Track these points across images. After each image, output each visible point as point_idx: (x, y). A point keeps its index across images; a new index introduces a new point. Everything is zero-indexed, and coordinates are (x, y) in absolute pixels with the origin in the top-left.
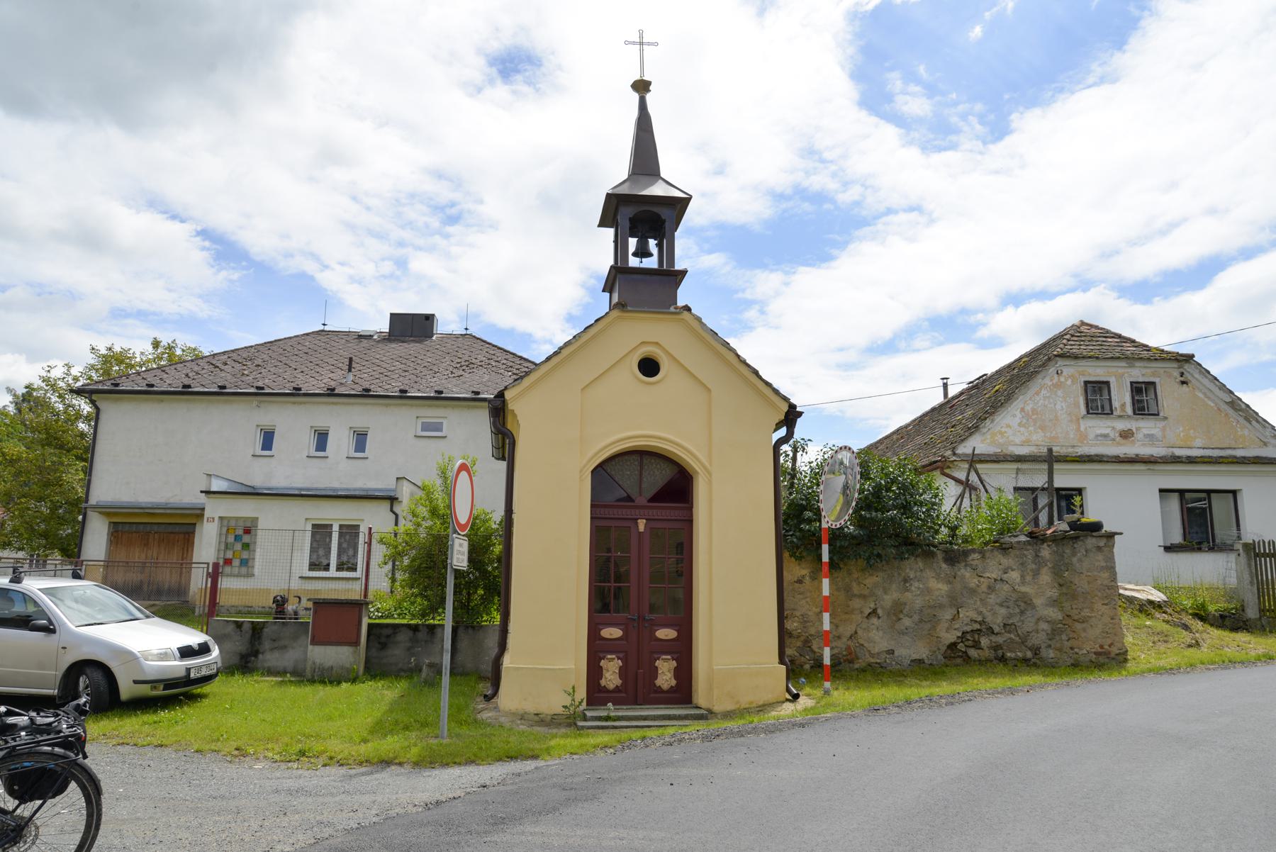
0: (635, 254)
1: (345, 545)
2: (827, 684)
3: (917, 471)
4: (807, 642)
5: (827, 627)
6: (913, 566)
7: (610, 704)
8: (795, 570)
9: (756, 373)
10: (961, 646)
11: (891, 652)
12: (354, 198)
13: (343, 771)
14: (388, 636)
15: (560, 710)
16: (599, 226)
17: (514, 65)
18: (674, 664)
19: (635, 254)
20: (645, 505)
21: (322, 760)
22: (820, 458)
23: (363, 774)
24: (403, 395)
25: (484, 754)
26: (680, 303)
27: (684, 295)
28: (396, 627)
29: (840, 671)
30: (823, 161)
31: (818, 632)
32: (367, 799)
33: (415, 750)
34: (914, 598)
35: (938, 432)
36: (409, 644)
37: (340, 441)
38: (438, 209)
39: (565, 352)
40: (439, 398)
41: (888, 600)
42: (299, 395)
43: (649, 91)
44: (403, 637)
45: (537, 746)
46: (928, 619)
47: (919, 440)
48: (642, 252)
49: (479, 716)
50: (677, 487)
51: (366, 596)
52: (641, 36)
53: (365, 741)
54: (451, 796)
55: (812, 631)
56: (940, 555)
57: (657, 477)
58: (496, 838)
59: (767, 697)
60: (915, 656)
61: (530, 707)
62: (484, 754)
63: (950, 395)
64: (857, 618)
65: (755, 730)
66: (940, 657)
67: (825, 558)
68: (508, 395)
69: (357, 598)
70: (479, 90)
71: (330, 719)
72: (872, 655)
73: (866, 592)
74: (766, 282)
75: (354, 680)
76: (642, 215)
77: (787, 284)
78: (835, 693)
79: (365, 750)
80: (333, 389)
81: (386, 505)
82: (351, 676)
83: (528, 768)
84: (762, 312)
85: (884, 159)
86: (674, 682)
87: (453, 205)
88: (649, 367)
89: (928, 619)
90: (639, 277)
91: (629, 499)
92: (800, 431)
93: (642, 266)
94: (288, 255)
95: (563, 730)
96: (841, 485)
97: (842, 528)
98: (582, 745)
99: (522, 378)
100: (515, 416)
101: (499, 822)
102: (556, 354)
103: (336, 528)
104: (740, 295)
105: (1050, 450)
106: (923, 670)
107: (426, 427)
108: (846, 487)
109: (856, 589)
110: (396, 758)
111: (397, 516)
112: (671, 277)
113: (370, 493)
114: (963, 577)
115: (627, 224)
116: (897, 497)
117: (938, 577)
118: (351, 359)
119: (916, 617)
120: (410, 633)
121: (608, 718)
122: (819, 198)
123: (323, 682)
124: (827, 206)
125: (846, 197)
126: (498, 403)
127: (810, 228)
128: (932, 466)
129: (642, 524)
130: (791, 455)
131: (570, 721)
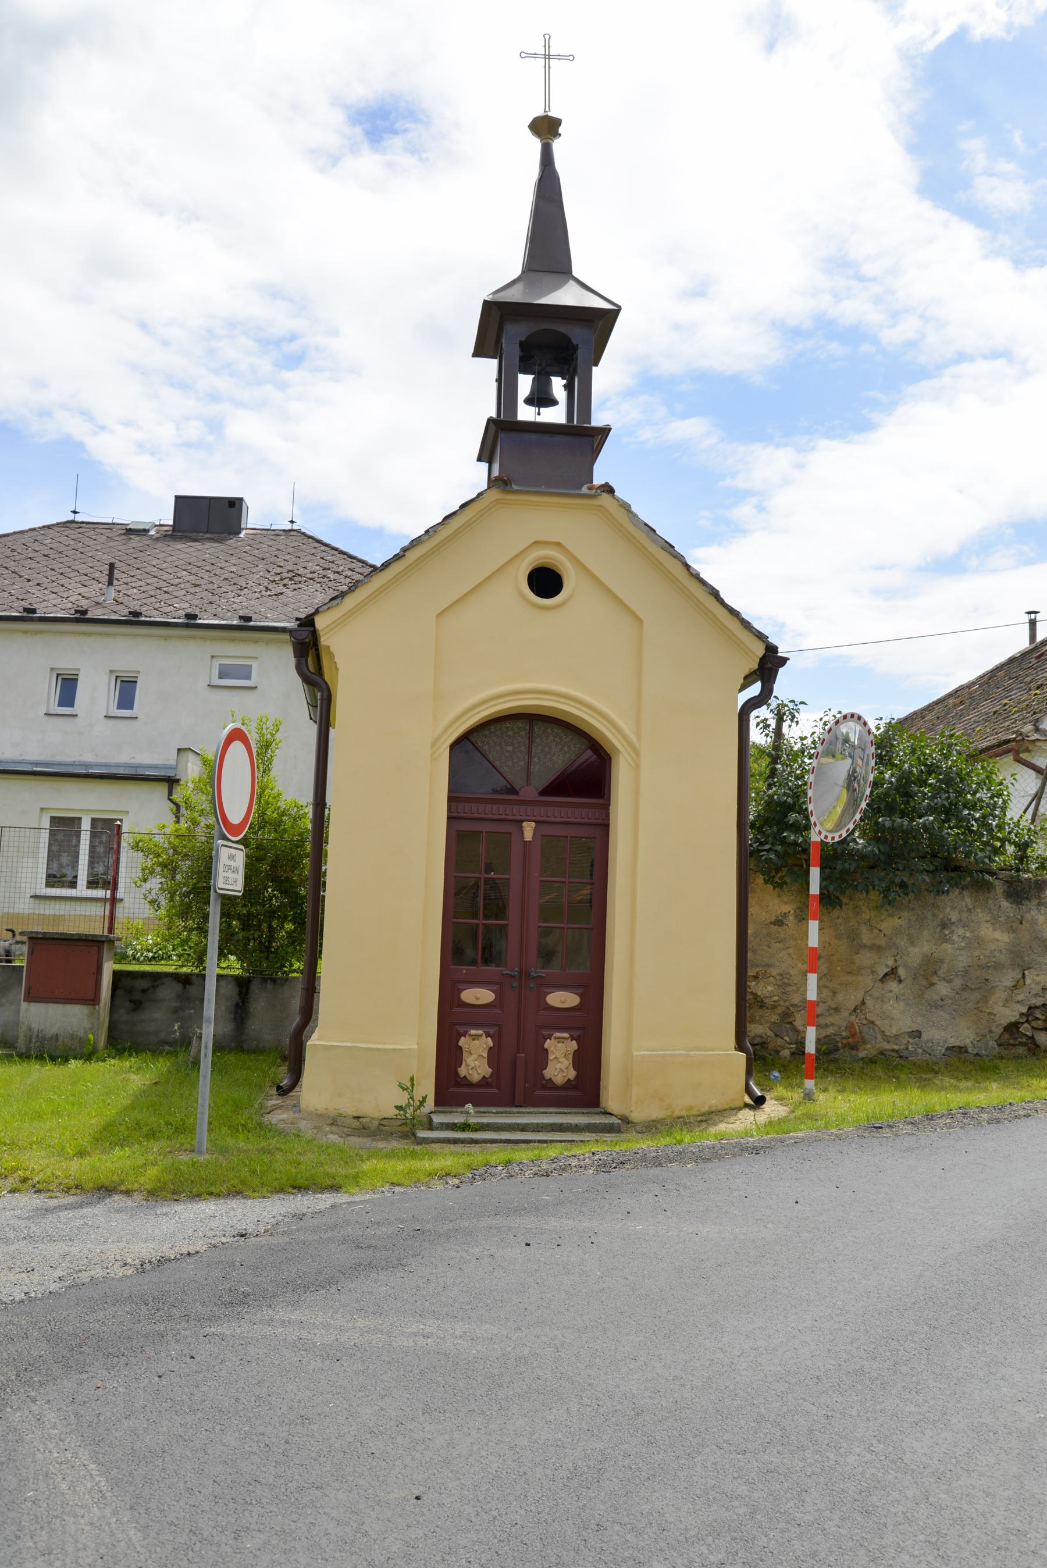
0: (529, 401)
1: (100, 849)
2: (809, 1084)
3: (973, 757)
4: (787, 1016)
5: (812, 995)
6: (956, 904)
7: (469, 1107)
8: (770, 904)
9: (715, 594)
10: (1025, 1029)
11: (917, 1034)
12: (144, 326)
13: (38, 1201)
14: (144, 991)
15: (392, 1112)
16: (475, 355)
17: (382, 122)
18: (574, 1045)
19: (529, 401)
20: (533, 802)
21: (12, 1182)
22: (819, 731)
23: (66, 1208)
24: (191, 622)
25: (256, 1181)
26: (598, 480)
27: (604, 469)
28: (156, 977)
29: (836, 1061)
30: (861, 278)
32: (56, 1250)
33: (152, 1172)
34: (956, 953)
35: (1015, 694)
36: (176, 1004)
37: (95, 692)
38: (269, 343)
39: (412, 556)
40: (245, 626)
41: (915, 954)
42: (32, 620)
43: (556, 134)
44: (167, 992)
45: (342, 1171)
46: (977, 985)
47: (987, 707)
48: (541, 398)
49: (267, 1118)
50: (586, 775)
51: (111, 930)
52: (547, 45)
53: (81, 1154)
54: (184, 1251)
55: (796, 999)
56: (999, 887)
57: (556, 758)
58: (225, 1329)
59: (715, 1101)
60: (953, 1042)
61: (347, 1106)
62: (256, 1181)
63: (1040, 638)
64: (866, 980)
65: (680, 1157)
66: (992, 1044)
67: (815, 888)
68: (320, 623)
69: (98, 932)
70: (335, 161)
71: (38, 1116)
72: (887, 1039)
73: (882, 942)
74: (767, 463)
75: (89, 1056)
76: (542, 335)
77: (800, 466)
78: (821, 1097)
79: (77, 1168)
80: (85, 612)
81: (162, 789)
82: (86, 1051)
83: (321, 1206)
84: (761, 509)
85: (953, 275)
86: (572, 1074)
87: (293, 338)
88: (545, 582)
89: (977, 985)
90: (534, 437)
91: (513, 791)
92: (784, 686)
93: (540, 419)
94: (45, 413)
95: (395, 1144)
96: (844, 775)
97: (843, 842)
98: (410, 1172)
99: (343, 595)
100: (331, 655)
101: (237, 1301)
102: (397, 558)
103: (86, 825)
104: (728, 482)
106: (964, 1063)
108: (852, 778)
109: (866, 937)
110: (122, 1182)
112: (584, 438)
113: (141, 772)
114: (1034, 922)
115: (517, 352)
116: (937, 791)
117: (995, 922)
118: (112, 566)
119: (958, 982)
120: (178, 987)
121: (465, 1127)
122: (854, 335)
123: (40, 1058)
124: (865, 348)
125: (892, 336)
126: (305, 634)
127: (834, 378)
128: (1001, 749)
129: (529, 830)
130: (773, 723)
131: (405, 1129)
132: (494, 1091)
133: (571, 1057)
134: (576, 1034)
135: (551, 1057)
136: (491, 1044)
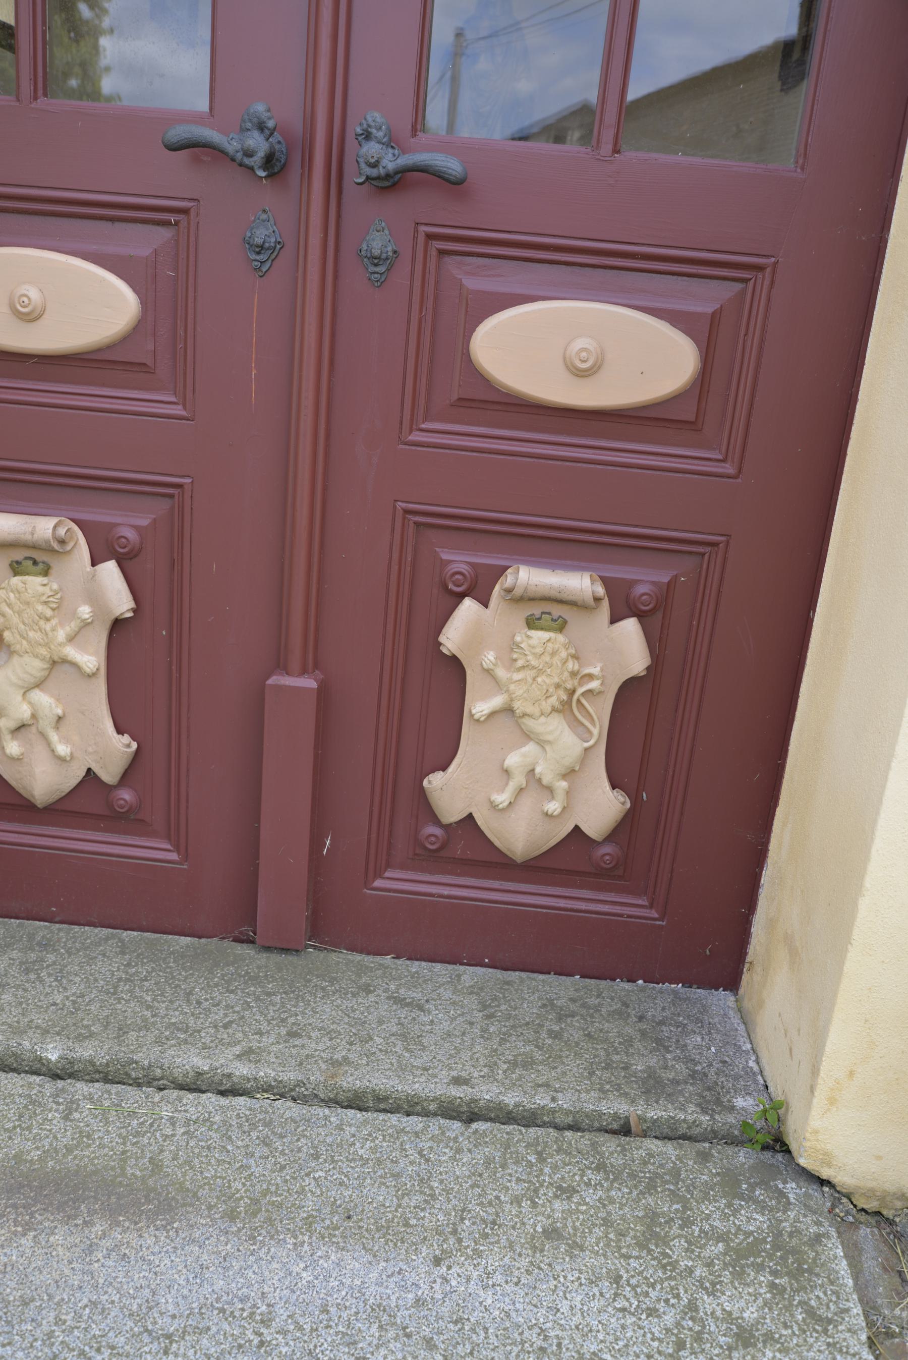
18: (628, 648)
86: (600, 807)
132: (157, 851)
133: (601, 712)
134: (647, 578)
135: (480, 705)
136: (121, 601)
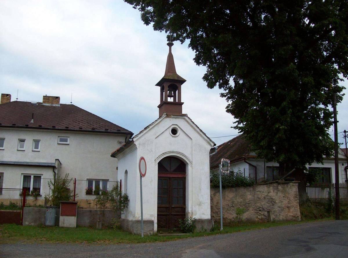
31: (330, 145)
42: (15, 127)
57: (174, 166)
80: (28, 125)
88: (174, 132)
105: (338, 122)
107: (61, 140)
111: (55, 173)
113: (16, 163)
